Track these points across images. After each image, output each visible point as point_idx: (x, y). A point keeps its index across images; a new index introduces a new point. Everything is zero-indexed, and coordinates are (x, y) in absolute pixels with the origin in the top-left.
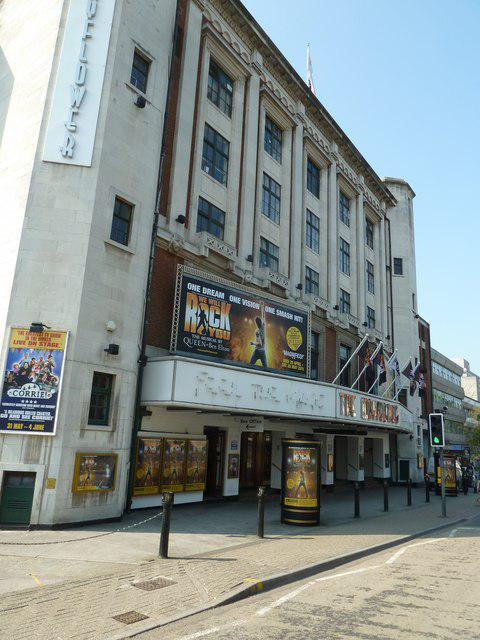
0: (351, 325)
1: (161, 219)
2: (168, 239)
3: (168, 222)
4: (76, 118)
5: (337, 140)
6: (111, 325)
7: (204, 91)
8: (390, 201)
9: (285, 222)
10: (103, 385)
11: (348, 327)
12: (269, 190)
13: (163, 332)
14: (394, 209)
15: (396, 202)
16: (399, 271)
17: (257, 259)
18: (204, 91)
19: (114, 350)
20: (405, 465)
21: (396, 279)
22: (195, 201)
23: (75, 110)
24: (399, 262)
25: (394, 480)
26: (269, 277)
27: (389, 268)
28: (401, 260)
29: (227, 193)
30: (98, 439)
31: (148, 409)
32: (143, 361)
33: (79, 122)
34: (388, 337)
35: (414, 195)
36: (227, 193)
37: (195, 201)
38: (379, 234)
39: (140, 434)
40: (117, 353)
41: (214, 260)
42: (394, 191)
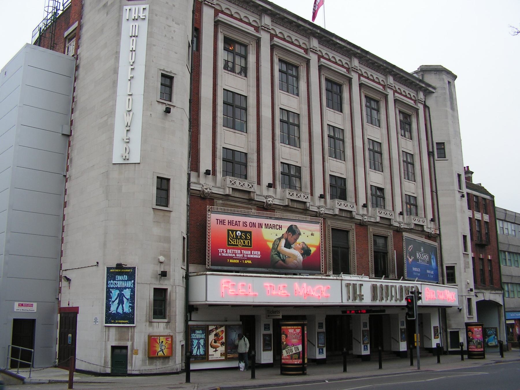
0: (341, 210)
1: (193, 174)
2: (200, 189)
3: (199, 176)
4: (129, 133)
5: (355, 55)
6: (162, 259)
7: (221, 64)
8: (428, 90)
9: (305, 144)
10: (160, 295)
11: (378, 219)
12: (287, 122)
13: (200, 253)
14: (434, 95)
15: (434, 88)
16: (442, 154)
17: (328, 196)
18: (221, 64)
19: (164, 274)
20: (455, 335)
21: (439, 164)
22: (220, 153)
23: (128, 129)
24: (441, 146)
25: (445, 349)
26: (378, 214)
27: (430, 154)
28: (168, 180)
29: (248, 138)
30: (160, 328)
31: (195, 307)
32: (187, 277)
33: (130, 135)
34: (432, 220)
35: (455, 77)
36: (248, 138)
37: (220, 153)
38: (418, 125)
39: (190, 323)
40: (166, 276)
41: (237, 195)
42: (430, 79)
